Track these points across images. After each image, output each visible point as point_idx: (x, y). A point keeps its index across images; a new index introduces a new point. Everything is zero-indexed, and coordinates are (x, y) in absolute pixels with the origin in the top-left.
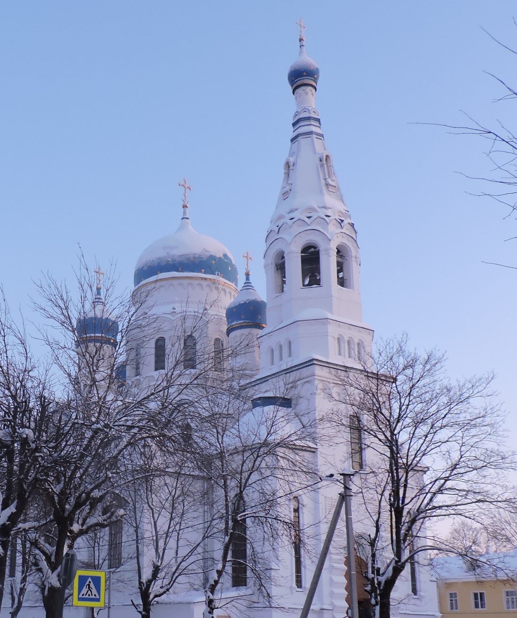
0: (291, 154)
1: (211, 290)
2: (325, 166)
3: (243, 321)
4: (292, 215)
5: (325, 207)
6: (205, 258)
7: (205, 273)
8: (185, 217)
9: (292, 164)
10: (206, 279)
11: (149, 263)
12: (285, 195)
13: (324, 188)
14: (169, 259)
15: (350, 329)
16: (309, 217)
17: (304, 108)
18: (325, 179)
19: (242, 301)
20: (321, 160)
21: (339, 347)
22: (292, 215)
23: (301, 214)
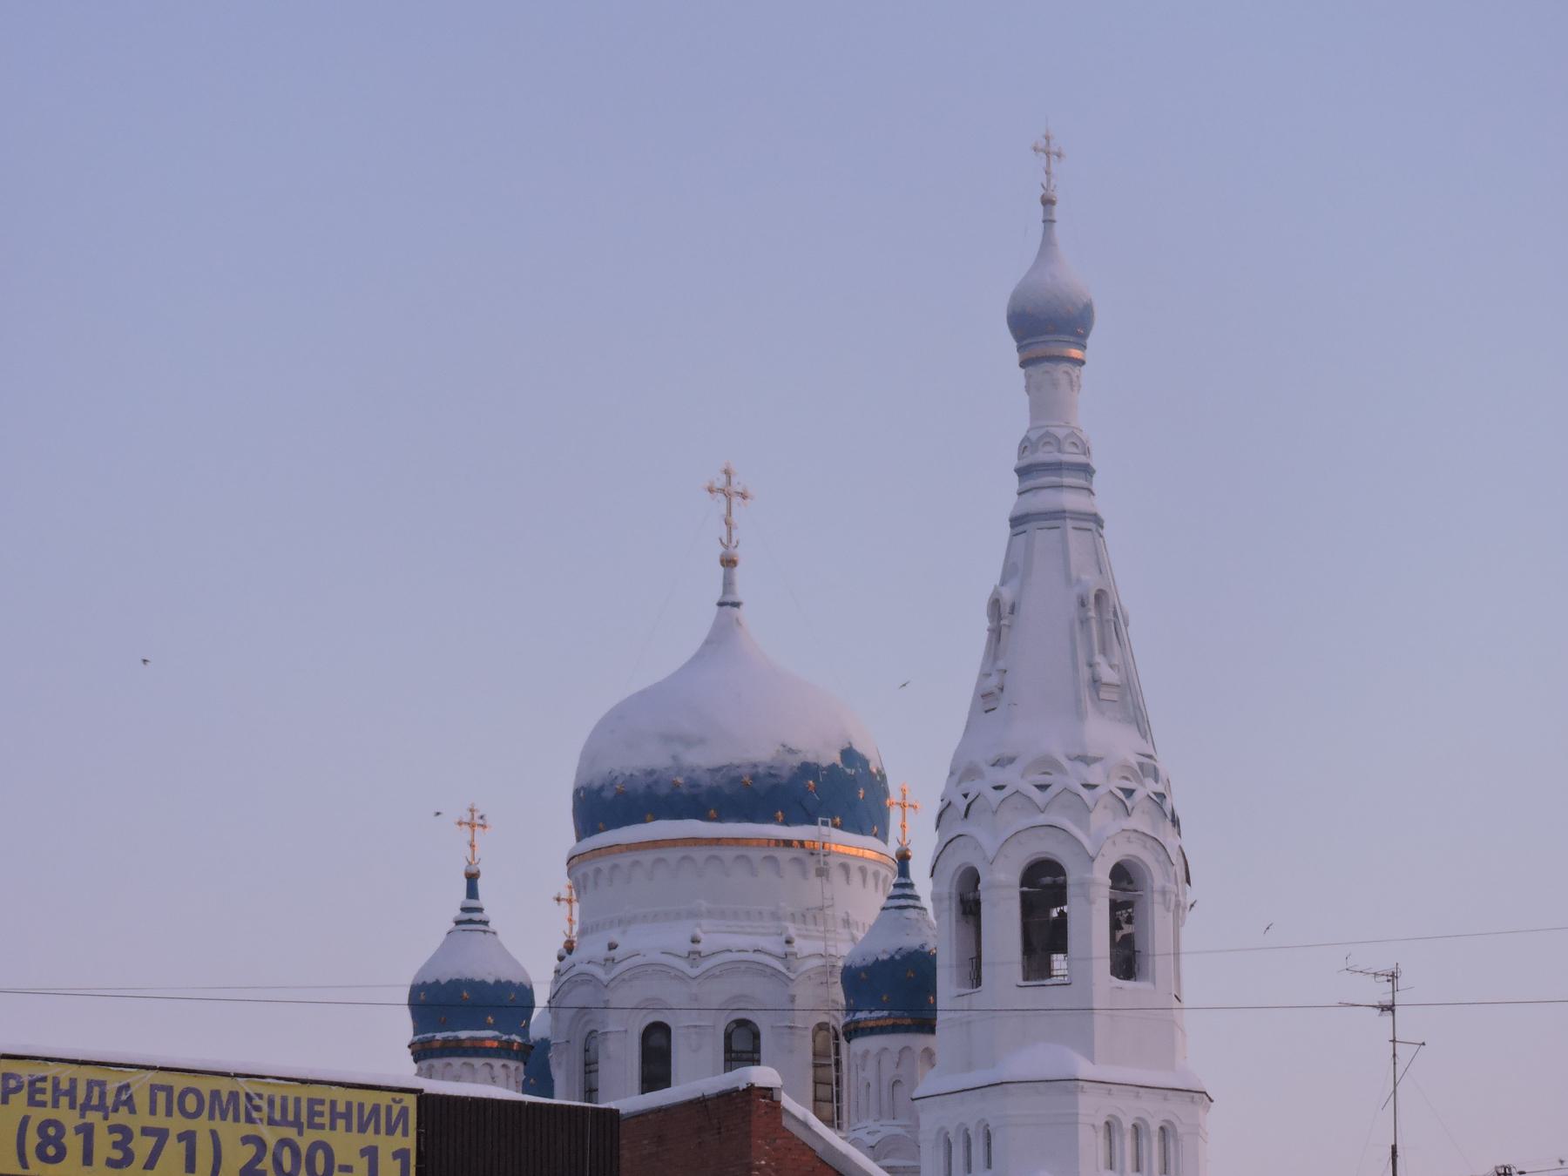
0: (1009, 573)
1: (804, 874)
2: (1094, 625)
3: (885, 1013)
4: (1000, 776)
5: (1085, 760)
6: (786, 773)
7: (786, 822)
8: (730, 599)
9: (1008, 610)
10: (788, 843)
11: (620, 781)
12: (988, 699)
13: (1086, 694)
14: (680, 780)
15: (1137, 1096)
16: (1042, 787)
17: (1047, 434)
18: (1091, 665)
19: (884, 952)
20: (1083, 604)
21: (1111, 1148)
22: (1000, 776)
23: (1022, 777)
